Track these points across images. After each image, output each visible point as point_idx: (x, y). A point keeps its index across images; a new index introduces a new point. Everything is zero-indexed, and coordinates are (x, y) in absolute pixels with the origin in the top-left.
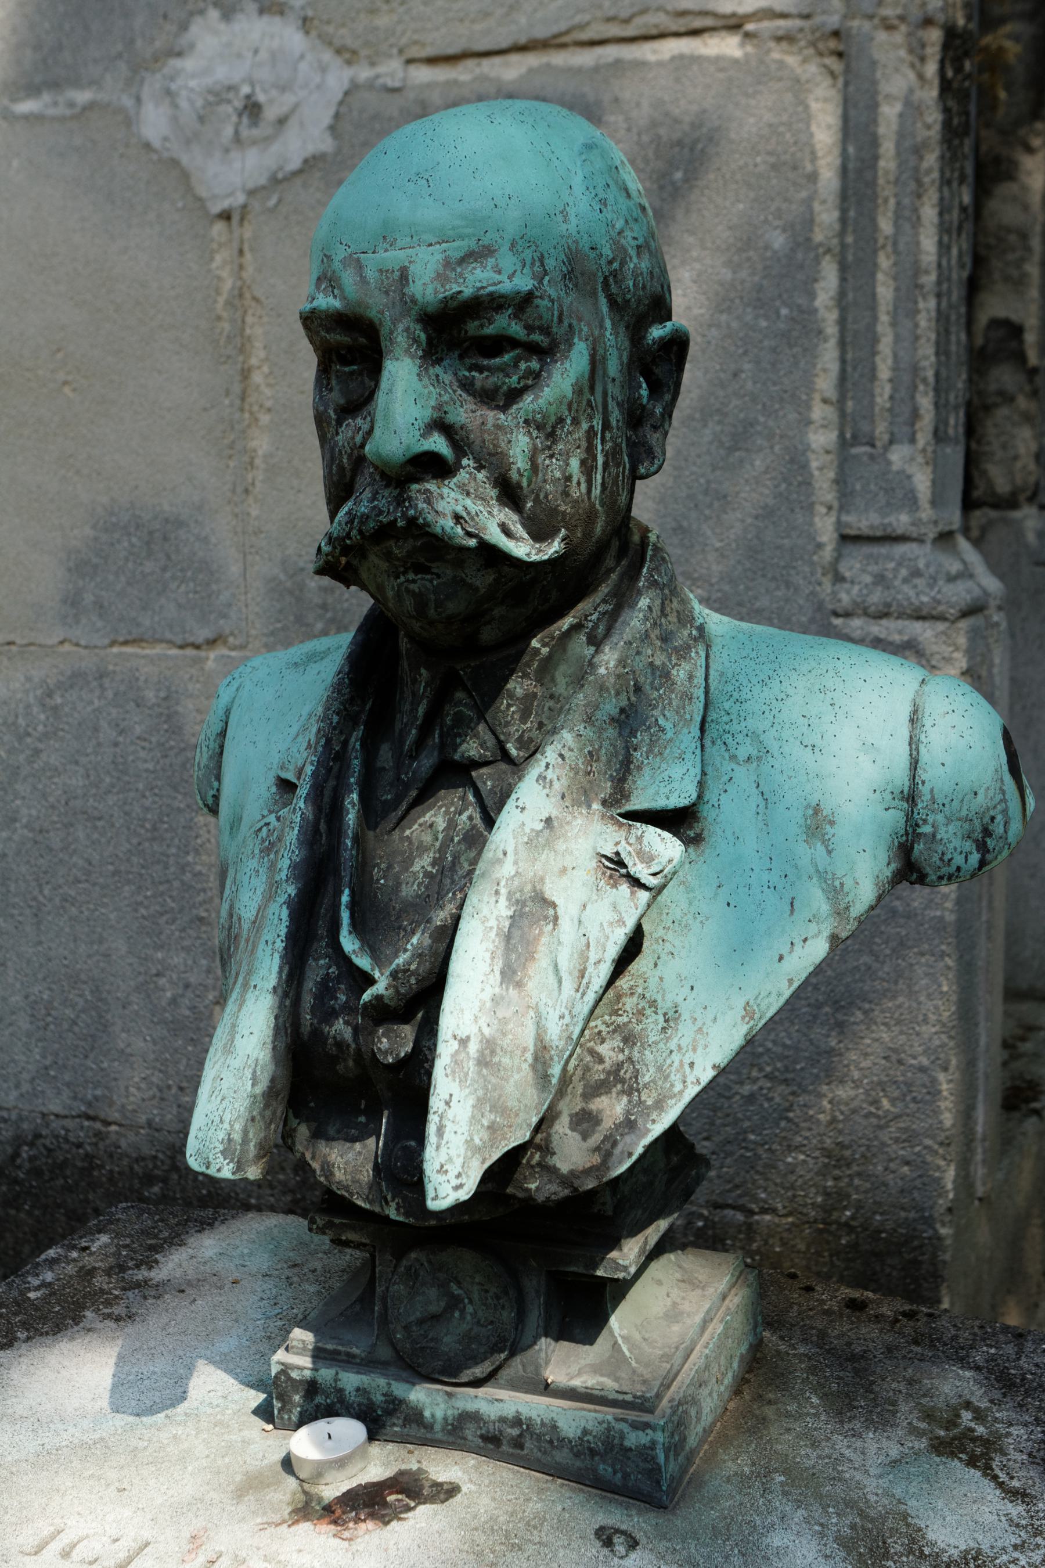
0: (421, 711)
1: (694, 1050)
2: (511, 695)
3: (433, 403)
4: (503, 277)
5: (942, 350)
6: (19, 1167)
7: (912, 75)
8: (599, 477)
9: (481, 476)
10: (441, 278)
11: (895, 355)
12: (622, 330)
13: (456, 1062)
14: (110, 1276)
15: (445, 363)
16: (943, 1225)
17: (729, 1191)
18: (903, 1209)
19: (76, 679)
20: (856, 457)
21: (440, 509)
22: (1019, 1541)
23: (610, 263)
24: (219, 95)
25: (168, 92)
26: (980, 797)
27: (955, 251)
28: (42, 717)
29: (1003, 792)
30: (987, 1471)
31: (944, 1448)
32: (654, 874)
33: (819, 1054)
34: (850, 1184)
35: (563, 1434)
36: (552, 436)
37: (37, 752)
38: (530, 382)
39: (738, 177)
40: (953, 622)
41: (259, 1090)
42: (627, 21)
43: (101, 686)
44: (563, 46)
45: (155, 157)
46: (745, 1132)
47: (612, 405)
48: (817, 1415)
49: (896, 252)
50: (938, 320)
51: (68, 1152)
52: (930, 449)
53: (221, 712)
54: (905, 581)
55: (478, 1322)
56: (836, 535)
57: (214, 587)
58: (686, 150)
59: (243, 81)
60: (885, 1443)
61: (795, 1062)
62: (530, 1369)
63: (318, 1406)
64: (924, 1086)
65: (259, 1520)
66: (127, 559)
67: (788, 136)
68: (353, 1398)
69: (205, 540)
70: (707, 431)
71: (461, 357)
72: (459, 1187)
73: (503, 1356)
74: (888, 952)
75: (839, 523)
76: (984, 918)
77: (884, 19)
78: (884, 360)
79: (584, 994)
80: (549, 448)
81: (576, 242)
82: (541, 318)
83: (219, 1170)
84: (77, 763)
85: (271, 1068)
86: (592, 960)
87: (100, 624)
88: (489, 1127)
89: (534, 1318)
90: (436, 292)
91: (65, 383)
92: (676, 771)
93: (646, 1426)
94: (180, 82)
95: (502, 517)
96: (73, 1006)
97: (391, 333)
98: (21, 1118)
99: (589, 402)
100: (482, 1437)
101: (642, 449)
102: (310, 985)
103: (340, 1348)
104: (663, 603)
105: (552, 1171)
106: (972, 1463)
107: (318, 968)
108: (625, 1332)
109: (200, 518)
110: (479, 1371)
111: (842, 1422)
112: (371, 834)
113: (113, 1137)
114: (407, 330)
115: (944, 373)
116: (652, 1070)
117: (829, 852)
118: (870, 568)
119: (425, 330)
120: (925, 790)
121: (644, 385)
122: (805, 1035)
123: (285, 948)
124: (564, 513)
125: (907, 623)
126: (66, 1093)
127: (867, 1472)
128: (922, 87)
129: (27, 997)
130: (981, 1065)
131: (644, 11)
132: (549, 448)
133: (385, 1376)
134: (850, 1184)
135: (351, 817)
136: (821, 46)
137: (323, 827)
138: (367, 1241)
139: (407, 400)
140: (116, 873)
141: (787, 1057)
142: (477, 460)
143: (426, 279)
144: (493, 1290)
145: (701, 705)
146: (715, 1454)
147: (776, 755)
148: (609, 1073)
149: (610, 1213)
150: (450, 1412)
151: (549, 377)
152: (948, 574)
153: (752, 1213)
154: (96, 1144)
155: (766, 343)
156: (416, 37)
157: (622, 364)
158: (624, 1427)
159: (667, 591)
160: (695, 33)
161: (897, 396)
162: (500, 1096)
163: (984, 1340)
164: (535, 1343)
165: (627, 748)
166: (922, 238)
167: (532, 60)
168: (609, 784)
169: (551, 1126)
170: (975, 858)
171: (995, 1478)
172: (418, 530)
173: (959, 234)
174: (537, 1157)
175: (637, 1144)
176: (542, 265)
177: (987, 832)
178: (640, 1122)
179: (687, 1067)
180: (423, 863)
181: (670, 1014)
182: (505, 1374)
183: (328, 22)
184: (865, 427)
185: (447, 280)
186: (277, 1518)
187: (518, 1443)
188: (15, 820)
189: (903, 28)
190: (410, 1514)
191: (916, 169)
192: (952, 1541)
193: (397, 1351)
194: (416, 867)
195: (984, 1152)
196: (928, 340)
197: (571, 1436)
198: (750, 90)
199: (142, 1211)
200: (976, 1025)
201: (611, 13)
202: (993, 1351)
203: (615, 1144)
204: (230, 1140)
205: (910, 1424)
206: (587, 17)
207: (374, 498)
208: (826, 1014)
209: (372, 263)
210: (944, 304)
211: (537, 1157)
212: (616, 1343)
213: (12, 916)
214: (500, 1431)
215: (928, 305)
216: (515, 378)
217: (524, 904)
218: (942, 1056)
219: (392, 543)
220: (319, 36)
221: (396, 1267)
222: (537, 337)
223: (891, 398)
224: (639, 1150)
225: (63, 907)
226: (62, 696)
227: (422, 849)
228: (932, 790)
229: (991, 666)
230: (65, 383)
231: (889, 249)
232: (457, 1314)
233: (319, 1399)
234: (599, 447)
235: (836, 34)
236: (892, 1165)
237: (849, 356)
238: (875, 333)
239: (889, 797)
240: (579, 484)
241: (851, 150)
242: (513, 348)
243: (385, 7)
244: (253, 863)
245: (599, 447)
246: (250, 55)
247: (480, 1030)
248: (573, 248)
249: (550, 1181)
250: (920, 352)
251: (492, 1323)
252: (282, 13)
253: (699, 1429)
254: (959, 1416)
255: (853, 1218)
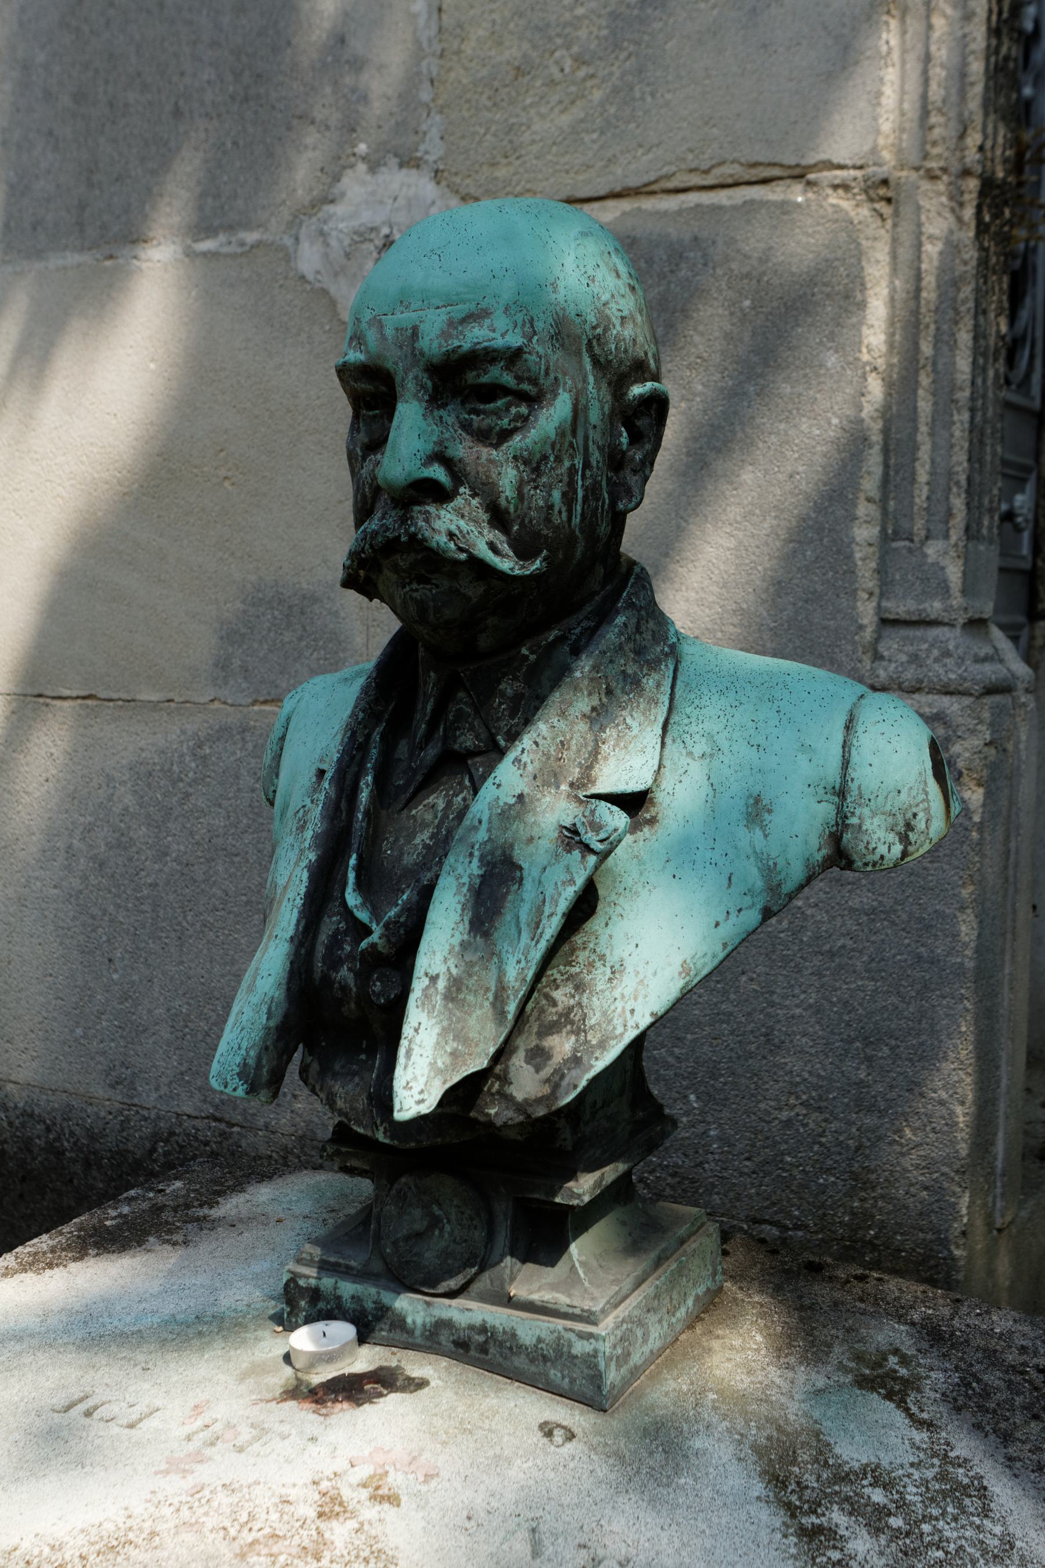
0: (429, 708)
1: (636, 999)
2: (503, 694)
3: (435, 439)
4: (497, 335)
5: (975, 457)
6: (155, 1161)
7: (951, 218)
8: (579, 508)
9: (475, 502)
10: (445, 335)
11: (933, 461)
12: (604, 386)
13: (426, 996)
14: (176, 1212)
15: (449, 407)
16: (958, 1247)
17: (767, 1208)
18: (922, 1230)
19: (223, 733)
20: (896, 550)
21: (436, 527)
22: (916, 1461)
23: (594, 328)
24: (363, 235)
25: (322, 233)
26: (904, 796)
27: (991, 373)
28: (193, 765)
29: (927, 794)
30: (902, 1405)
31: (864, 1383)
32: (601, 841)
33: (849, 1085)
34: (875, 1206)
35: (521, 1342)
36: (537, 470)
37: (187, 795)
38: (519, 424)
39: (798, 304)
40: (978, 698)
41: (272, 1023)
42: (706, 172)
43: (243, 739)
44: (653, 193)
45: (308, 287)
46: (783, 1154)
47: (592, 447)
48: (758, 1350)
49: (935, 371)
50: (971, 432)
51: (197, 1149)
52: (961, 544)
53: (283, 720)
54: (936, 660)
55: (454, 1241)
56: (876, 619)
57: (341, 655)
58: (754, 281)
59: (384, 223)
60: (814, 1375)
61: (828, 1092)
62: (497, 1283)
63: (320, 1311)
64: (943, 1117)
65: (254, 1397)
66: (270, 630)
67: (842, 269)
68: (349, 1305)
69: (336, 614)
70: (766, 525)
71: (463, 403)
72: (422, 1101)
73: (474, 1270)
74: (913, 994)
75: (879, 606)
76: (1007, 971)
77: (928, 170)
78: (923, 466)
79: (537, 942)
80: (534, 480)
81: (564, 309)
82: (529, 370)
83: (235, 1090)
84: (220, 806)
85: (285, 1005)
86: (546, 914)
87: (244, 685)
88: (451, 1054)
89: (502, 1238)
90: (440, 346)
91: (226, 478)
92: (637, 761)
93: (590, 1336)
94: (331, 225)
95: (491, 537)
96: (207, 1019)
97: (403, 380)
98: (158, 1117)
99: (571, 443)
100: (454, 1342)
101: (622, 489)
102: (323, 938)
103: (341, 1261)
104: (638, 623)
105: (509, 1098)
106: (889, 1396)
107: (330, 924)
108: (584, 1258)
109: (332, 595)
110: (453, 1283)
111: (779, 1357)
112: (384, 812)
113: (236, 1137)
114: (416, 378)
115: (977, 478)
116: (598, 1014)
117: (766, 836)
118: (906, 649)
119: (430, 378)
120: (853, 786)
121: (625, 434)
122: (837, 1067)
123: (303, 905)
124: (546, 537)
125: (936, 697)
126: (198, 1096)
127: (792, 1397)
128: (960, 229)
129: (168, 1010)
130: (1002, 1107)
131: (721, 163)
132: (534, 480)
133: (377, 1286)
134: (875, 1206)
135: (364, 796)
136: (871, 192)
137: (343, 805)
138: (367, 1168)
139: (412, 436)
140: (247, 903)
141: (821, 1087)
142: (472, 489)
143: (433, 335)
144: (468, 1212)
145: (665, 709)
146: (659, 1373)
147: (726, 752)
148: (561, 1015)
149: (570, 1148)
150: (428, 1320)
151: (536, 420)
152: (976, 655)
153: (786, 1228)
154: (221, 1143)
155: (819, 448)
156: (528, 186)
157: (604, 414)
158: (572, 1337)
159: (643, 613)
160: (765, 181)
161: (933, 497)
162: (463, 1028)
163: (923, 1302)
164: (501, 1261)
165: (596, 741)
166: (958, 359)
167: (626, 205)
168: (577, 770)
169: (509, 1059)
170: (897, 849)
171: (907, 1410)
172: (417, 543)
173: (996, 360)
174: (497, 1086)
175: (581, 1078)
176: (532, 326)
177: (909, 827)
178: (585, 1058)
179: (628, 1013)
180: (423, 837)
181: (617, 967)
182: (476, 1287)
183: (456, 174)
184: (905, 524)
185: (451, 336)
186: (270, 1396)
187: (483, 1349)
188: (166, 854)
189: (945, 178)
190: (381, 1400)
191: (954, 300)
192: (856, 1456)
193: (386, 1264)
194: (417, 841)
195: (1003, 1186)
196: (962, 448)
197: (528, 1343)
198: (810, 231)
199: (215, 1165)
200: (998, 1068)
201: (693, 166)
202: (930, 1312)
203: (563, 1076)
204: (245, 1064)
205: (840, 1362)
206: (674, 168)
207: (383, 518)
208: (857, 1049)
209: (390, 324)
210: (978, 418)
211: (497, 1086)
212: (573, 1266)
213: (160, 938)
214: (469, 1338)
215: (962, 418)
216: (506, 421)
217: (494, 865)
218: (959, 1090)
219: (398, 556)
220: (448, 186)
221: (390, 1190)
222: (525, 386)
223: (928, 498)
224: (583, 1083)
225: (202, 932)
226: (211, 747)
227: (424, 825)
228: (859, 787)
229: (1018, 742)
230: (226, 478)
231: (929, 368)
232: (437, 1232)
233: (321, 1305)
234: (580, 483)
235: (885, 182)
236: (912, 1190)
237: (892, 462)
238: (915, 441)
239: (821, 791)
240: (560, 512)
241: (897, 283)
242: (505, 396)
243: (504, 161)
244: (290, 839)
245: (580, 483)
246: (390, 201)
247: (448, 969)
248: (561, 314)
249: (507, 1108)
250: (954, 459)
251: (466, 1241)
252: (418, 167)
253: (647, 1349)
254: (886, 1360)
255: (876, 1237)
